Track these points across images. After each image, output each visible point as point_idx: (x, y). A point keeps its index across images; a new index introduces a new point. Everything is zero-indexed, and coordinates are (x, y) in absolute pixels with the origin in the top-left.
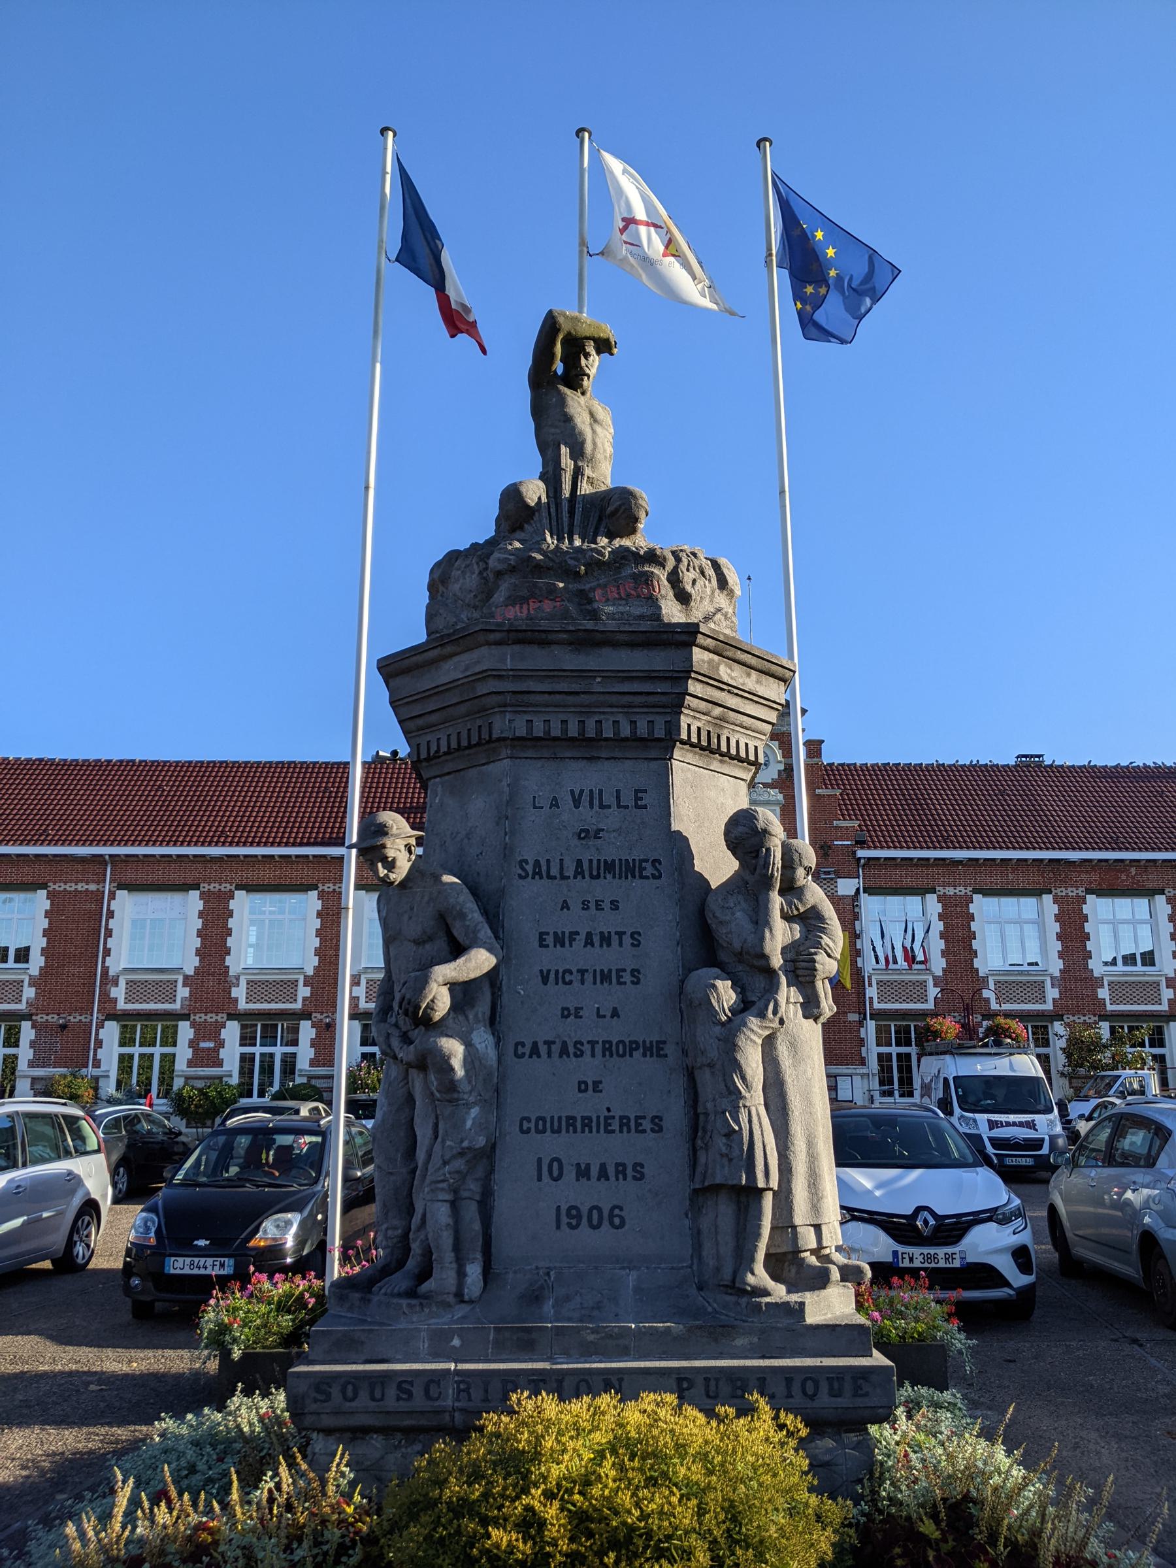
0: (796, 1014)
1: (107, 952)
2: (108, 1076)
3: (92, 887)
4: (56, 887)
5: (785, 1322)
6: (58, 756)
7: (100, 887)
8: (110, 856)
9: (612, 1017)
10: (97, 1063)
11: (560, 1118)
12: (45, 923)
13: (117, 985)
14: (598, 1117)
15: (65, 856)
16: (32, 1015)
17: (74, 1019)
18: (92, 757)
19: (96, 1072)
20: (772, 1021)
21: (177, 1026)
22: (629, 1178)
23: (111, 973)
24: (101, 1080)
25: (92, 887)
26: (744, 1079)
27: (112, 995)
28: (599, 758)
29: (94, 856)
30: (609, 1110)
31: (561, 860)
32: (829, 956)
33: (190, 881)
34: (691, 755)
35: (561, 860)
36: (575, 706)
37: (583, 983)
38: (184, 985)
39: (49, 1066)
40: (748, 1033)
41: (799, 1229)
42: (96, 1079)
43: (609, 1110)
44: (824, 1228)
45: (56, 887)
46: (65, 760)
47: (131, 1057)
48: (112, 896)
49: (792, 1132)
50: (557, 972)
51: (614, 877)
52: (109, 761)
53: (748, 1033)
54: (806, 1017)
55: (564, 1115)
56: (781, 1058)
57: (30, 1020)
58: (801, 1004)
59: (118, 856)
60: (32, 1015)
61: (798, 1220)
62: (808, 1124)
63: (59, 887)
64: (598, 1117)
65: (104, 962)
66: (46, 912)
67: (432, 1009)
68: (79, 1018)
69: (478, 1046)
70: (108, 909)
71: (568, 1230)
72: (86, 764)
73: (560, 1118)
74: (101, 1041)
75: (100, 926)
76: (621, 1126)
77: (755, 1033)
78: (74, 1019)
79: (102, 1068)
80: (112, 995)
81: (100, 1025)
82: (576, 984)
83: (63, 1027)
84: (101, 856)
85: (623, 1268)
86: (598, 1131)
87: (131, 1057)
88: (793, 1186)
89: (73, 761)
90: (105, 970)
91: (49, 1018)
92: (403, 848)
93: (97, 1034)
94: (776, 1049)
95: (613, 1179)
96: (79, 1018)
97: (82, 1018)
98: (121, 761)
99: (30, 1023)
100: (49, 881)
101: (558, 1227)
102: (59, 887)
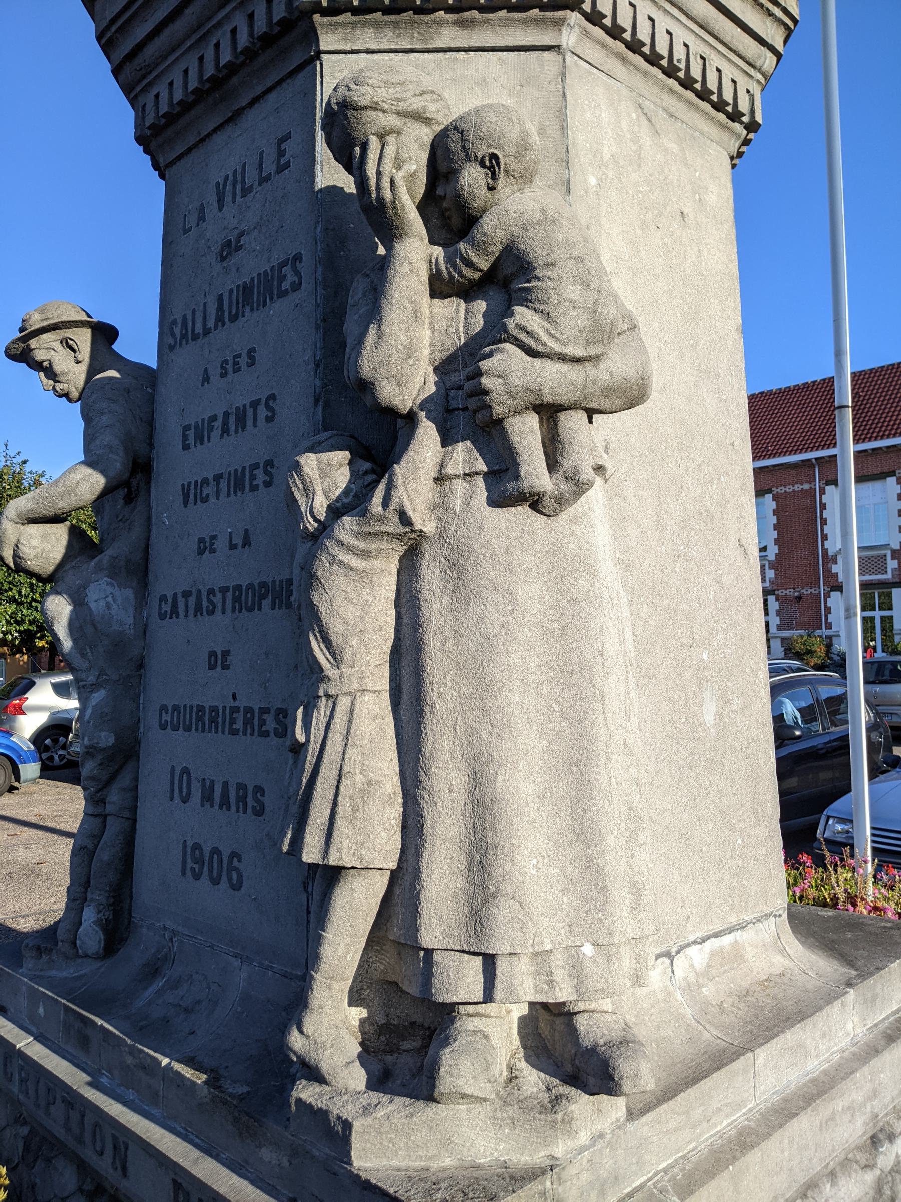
0: (468, 499)
1: (825, 537)
2: (839, 635)
3: (806, 486)
4: (779, 490)
5: (321, 1150)
6: (774, 387)
7: (812, 486)
8: (816, 459)
9: (244, 547)
10: (829, 626)
11: (191, 707)
12: (774, 520)
13: (836, 563)
14: (224, 707)
15: (782, 465)
16: (774, 591)
17: (807, 591)
18: (800, 382)
19: (829, 632)
20: (382, 520)
21: (891, 593)
22: (249, 811)
23: (830, 554)
24: (834, 638)
25: (806, 486)
26: (327, 640)
27: (834, 571)
28: (244, 108)
29: (803, 461)
30: (234, 697)
31: (205, 304)
32: (531, 353)
33: (886, 469)
34: (370, 32)
35: (205, 304)
36: (187, 36)
37: (218, 499)
38: (893, 558)
39: (792, 629)
40: (335, 550)
41: (437, 957)
42: (830, 637)
43: (234, 697)
44: (501, 966)
45: (779, 490)
46: (781, 389)
47: (873, 618)
48: (822, 492)
49: (427, 750)
50: (196, 482)
51: (252, 309)
52: (814, 382)
53: (335, 550)
54: (494, 502)
55: (195, 703)
56: (425, 595)
57: (774, 594)
58: (486, 476)
59: (823, 458)
60: (774, 591)
61: (430, 936)
62: (472, 733)
63: (781, 490)
64: (224, 707)
65: (823, 545)
66: (774, 511)
67: (20, 558)
68: (810, 591)
69: (93, 605)
70: (821, 502)
71: (191, 879)
72: (797, 388)
73: (191, 707)
74: (830, 608)
75: (816, 517)
76: (245, 725)
77: (349, 549)
78: (807, 591)
79: (834, 629)
80: (834, 571)
81: (828, 596)
82: (212, 499)
83: (799, 598)
84: (809, 460)
85: (236, 956)
86: (223, 733)
87: (873, 618)
88: (424, 864)
89: (795, 386)
90: (825, 552)
91: (787, 592)
92: (57, 345)
93: (826, 603)
94: (418, 577)
95: (233, 808)
96: (810, 591)
97: (813, 591)
98: (824, 380)
99: (773, 597)
100: (773, 486)
101: (184, 873)
102: (781, 490)
